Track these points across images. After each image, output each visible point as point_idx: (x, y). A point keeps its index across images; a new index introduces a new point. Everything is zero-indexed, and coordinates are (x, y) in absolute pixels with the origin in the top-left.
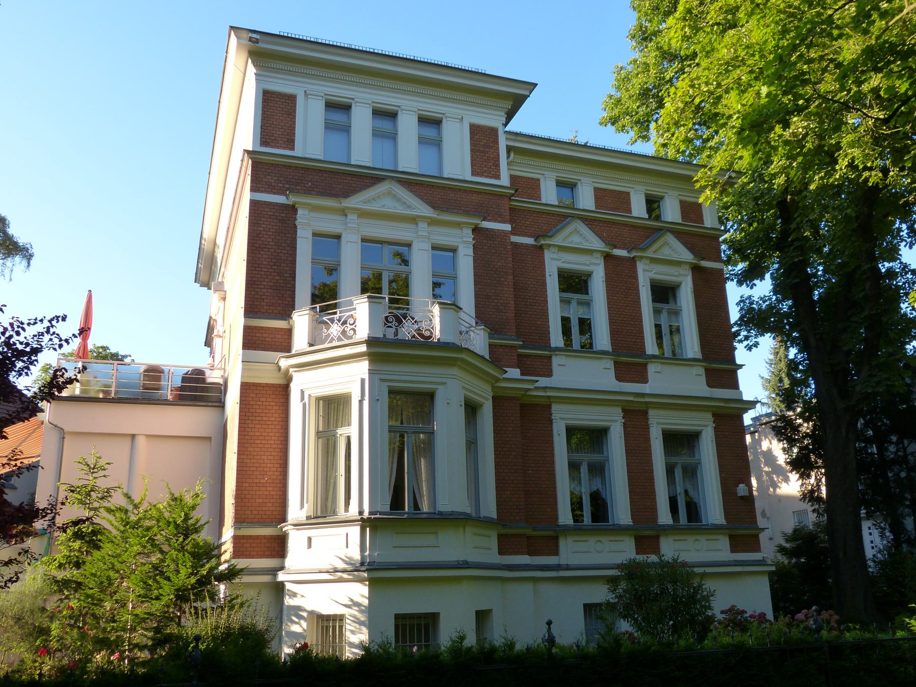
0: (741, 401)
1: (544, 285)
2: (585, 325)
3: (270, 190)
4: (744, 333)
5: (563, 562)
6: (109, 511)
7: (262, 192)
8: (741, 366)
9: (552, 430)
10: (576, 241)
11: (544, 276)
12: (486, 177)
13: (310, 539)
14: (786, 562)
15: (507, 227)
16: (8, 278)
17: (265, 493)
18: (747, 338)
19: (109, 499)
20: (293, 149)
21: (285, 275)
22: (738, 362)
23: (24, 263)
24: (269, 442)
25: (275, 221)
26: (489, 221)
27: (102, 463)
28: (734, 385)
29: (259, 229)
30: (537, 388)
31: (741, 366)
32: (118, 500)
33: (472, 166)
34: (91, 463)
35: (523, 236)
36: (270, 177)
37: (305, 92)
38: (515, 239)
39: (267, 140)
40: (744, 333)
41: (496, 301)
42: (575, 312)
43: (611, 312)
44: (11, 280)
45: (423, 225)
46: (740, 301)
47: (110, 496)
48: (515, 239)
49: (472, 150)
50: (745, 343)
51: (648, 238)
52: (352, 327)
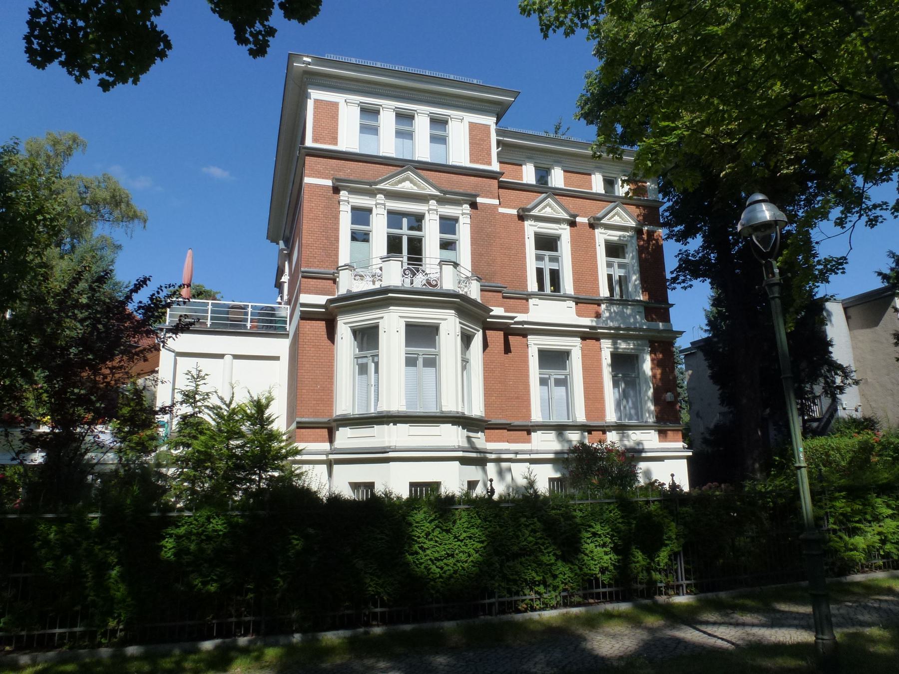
0: (671, 331)
1: (524, 245)
2: (555, 276)
3: (319, 175)
4: (682, 278)
5: (535, 448)
6: (207, 407)
7: (314, 177)
8: (672, 305)
9: (528, 353)
10: (548, 212)
11: (524, 238)
12: (481, 164)
13: (277, 358)
14: (710, 451)
15: (496, 202)
16: (129, 236)
17: (318, 397)
18: (684, 281)
19: (209, 400)
20: (336, 144)
21: (331, 239)
22: (670, 302)
23: (142, 225)
24: (321, 361)
25: (323, 198)
26: (483, 197)
27: (202, 374)
28: (666, 318)
29: (312, 205)
30: (516, 323)
31: (672, 305)
32: (214, 401)
33: (470, 155)
34: (194, 373)
35: (509, 208)
36: (320, 166)
37: (346, 101)
38: (501, 210)
39: (318, 138)
40: (682, 278)
41: (486, 257)
42: (547, 266)
43: (486, 369)
44: (131, 237)
45: (433, 202)
46: (679, 254)
47: (209, 398)
48: (501, 210)
49: (470, 143)
50: (683, 285)
51: (604, 208)
52: (379, 278)
